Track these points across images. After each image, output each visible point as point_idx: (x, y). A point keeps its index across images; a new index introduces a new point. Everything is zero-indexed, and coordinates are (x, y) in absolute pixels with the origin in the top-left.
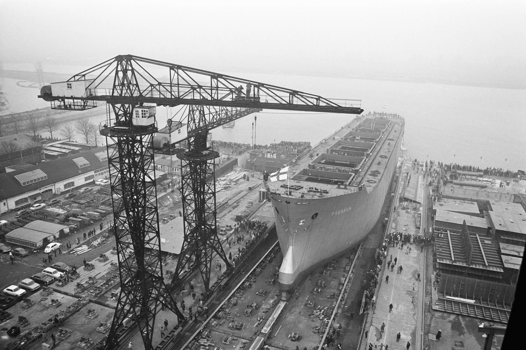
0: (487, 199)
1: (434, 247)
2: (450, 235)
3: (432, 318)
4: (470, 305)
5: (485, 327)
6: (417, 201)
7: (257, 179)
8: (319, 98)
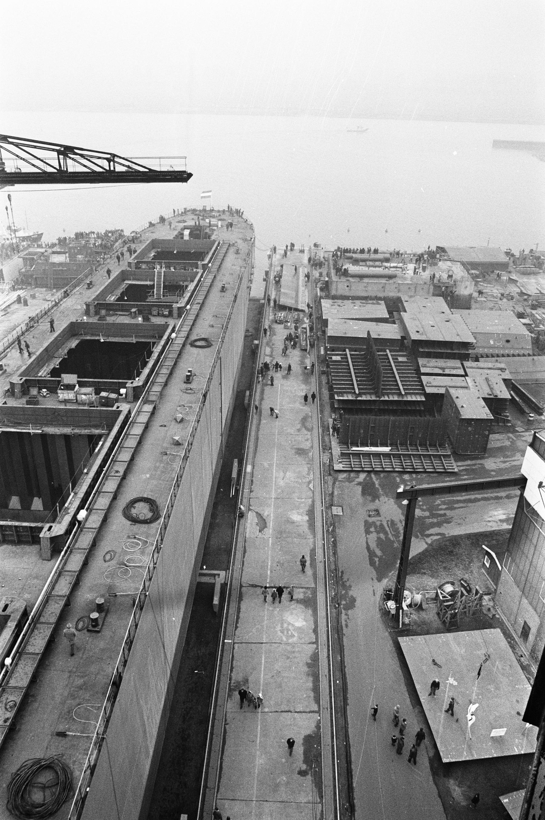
0: (399, 295)
1: (330, 377)
2: (351, 355)
3: (334, 483)
4: (386, 455)
5: (405, 491)
6: (300, 308)
7: (41, 301)
8: (112, 158)
